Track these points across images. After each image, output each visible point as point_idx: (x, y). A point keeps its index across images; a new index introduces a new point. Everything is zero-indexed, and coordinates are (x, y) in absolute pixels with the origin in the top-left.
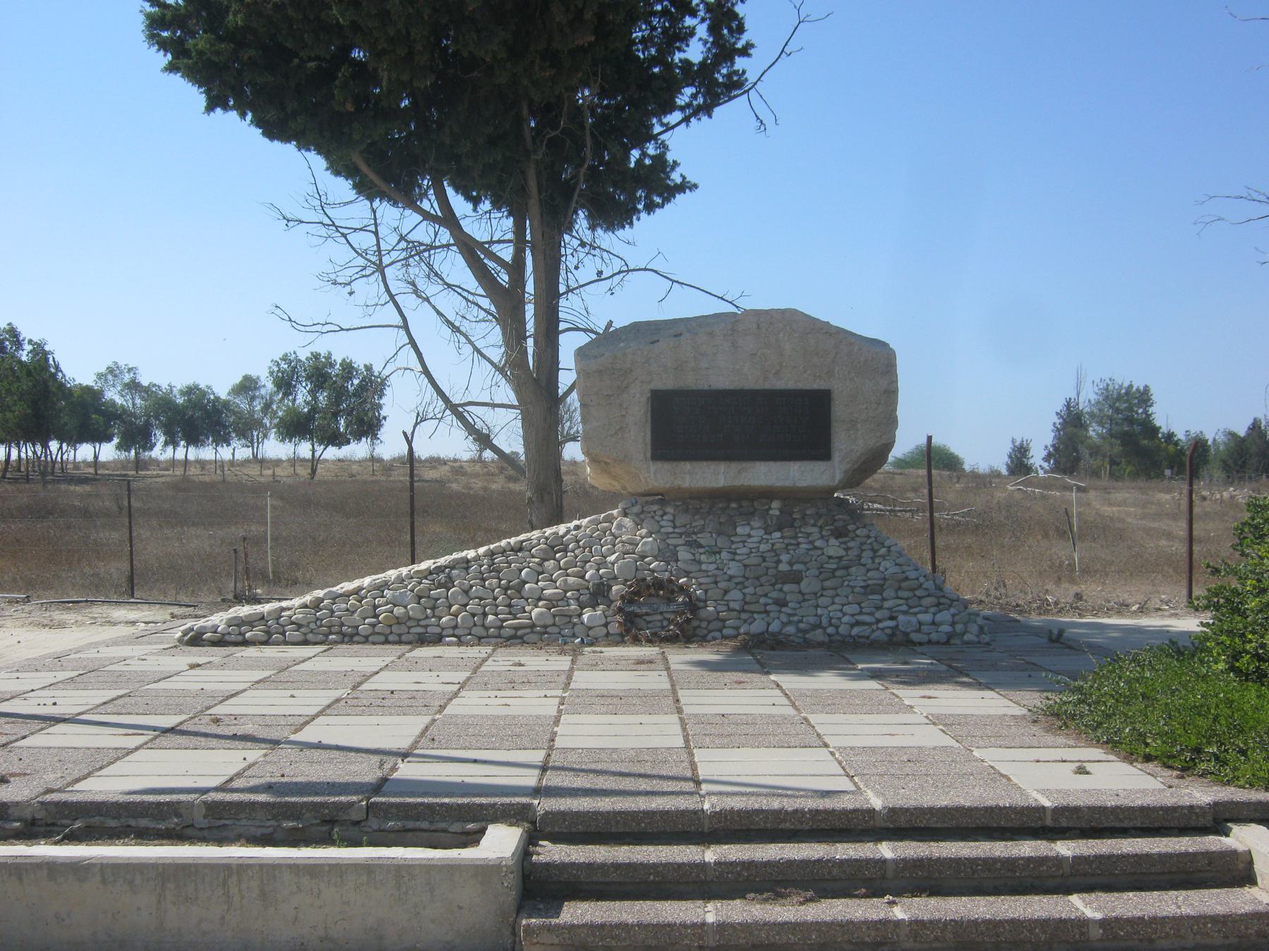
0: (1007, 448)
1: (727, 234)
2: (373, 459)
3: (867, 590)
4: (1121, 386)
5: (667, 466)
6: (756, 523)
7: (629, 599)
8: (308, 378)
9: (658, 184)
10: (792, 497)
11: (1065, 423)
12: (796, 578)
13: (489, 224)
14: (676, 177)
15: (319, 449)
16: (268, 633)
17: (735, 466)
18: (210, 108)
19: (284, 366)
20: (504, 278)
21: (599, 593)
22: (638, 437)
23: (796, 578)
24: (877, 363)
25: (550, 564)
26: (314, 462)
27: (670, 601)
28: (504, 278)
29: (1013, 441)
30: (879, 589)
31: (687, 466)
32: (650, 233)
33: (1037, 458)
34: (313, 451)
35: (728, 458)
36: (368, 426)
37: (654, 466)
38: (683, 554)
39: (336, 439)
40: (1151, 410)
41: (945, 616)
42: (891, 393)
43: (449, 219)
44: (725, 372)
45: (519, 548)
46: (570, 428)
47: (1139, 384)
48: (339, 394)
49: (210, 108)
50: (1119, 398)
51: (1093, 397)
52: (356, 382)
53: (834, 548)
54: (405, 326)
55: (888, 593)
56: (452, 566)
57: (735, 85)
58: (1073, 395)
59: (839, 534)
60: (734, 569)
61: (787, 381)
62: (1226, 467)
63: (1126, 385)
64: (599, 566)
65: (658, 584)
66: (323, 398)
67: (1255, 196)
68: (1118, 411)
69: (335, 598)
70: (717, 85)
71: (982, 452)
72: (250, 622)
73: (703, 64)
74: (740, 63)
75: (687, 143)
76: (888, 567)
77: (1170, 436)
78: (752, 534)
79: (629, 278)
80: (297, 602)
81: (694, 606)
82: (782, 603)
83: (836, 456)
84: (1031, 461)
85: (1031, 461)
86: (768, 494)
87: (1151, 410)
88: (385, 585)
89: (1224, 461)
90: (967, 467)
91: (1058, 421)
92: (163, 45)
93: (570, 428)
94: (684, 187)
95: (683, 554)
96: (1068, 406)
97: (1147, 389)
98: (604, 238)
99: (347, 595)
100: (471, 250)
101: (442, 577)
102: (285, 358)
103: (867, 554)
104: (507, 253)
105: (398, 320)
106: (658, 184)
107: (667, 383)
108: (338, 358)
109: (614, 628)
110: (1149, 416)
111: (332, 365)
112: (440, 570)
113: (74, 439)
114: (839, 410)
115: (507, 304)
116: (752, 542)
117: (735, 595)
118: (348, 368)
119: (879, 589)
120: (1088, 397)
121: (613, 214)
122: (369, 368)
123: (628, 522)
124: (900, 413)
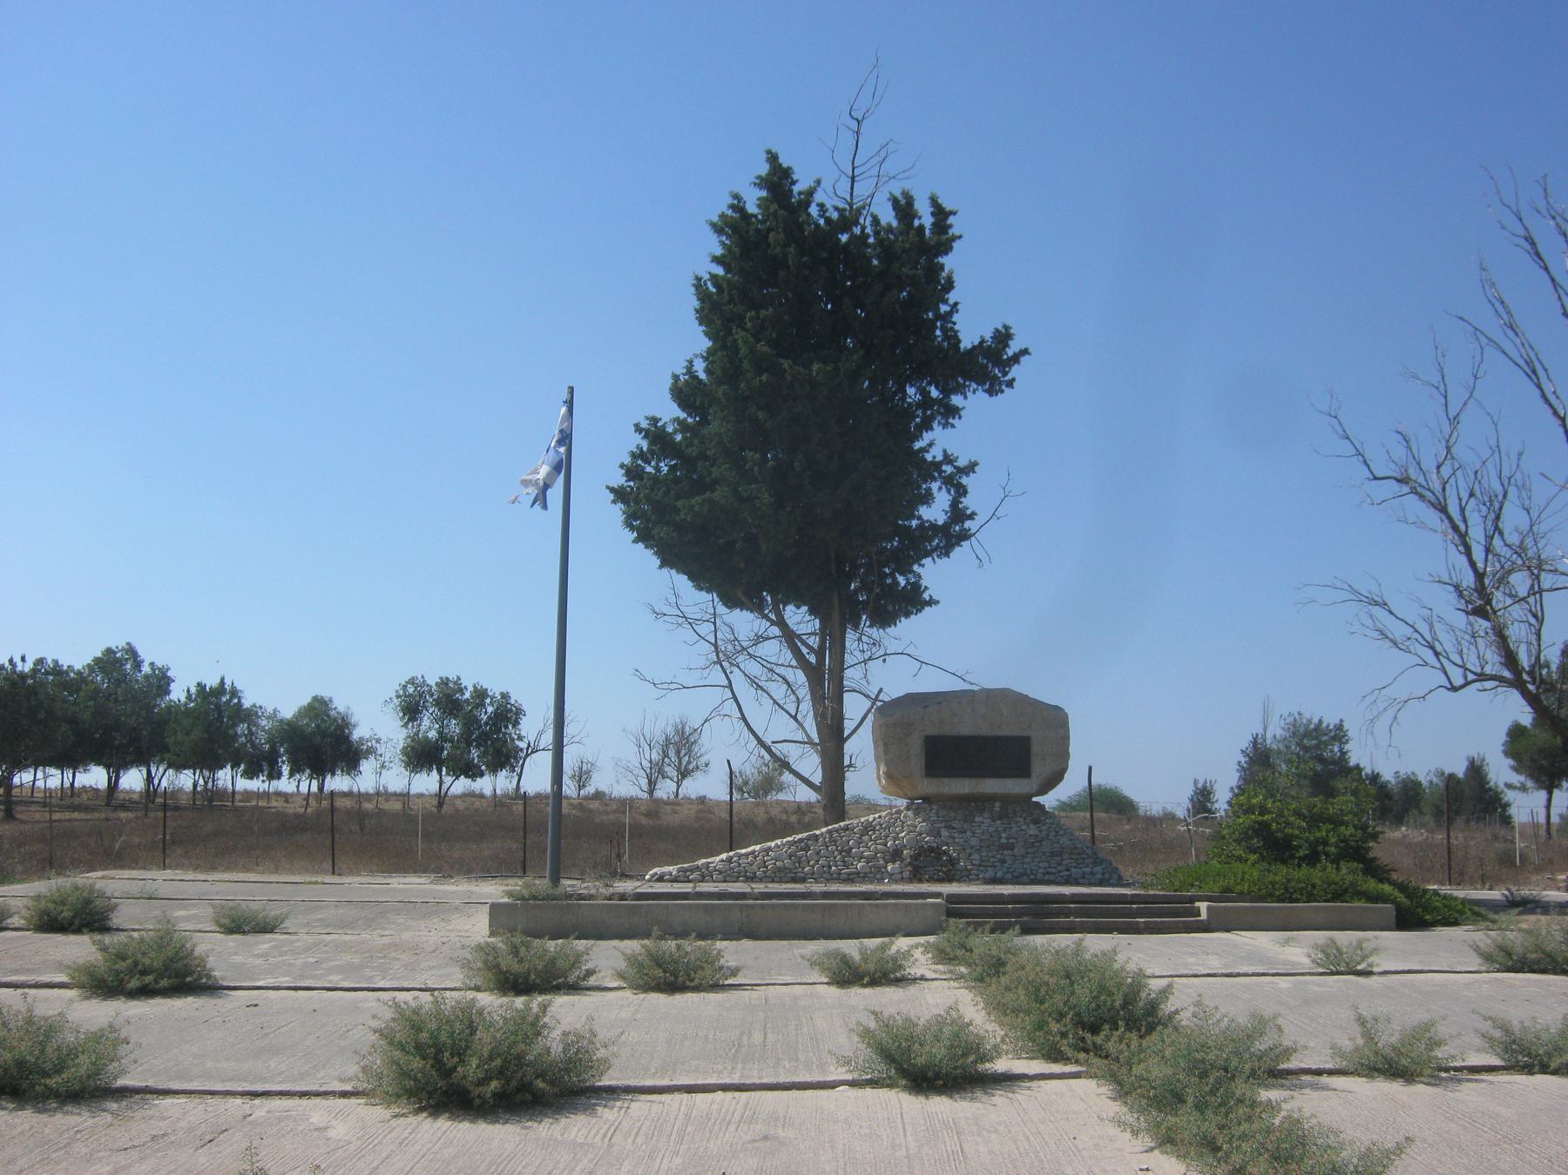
0: (1189, 791)
1: (954, 638)
2: (520, 796)
3: (1053, 854)
4: (1310, 721)
5: (935, 781)
6: (986, 815)
7: (915, 858)
8: (437, 703)
9: (913, 600)
10: (1007, 800)
11: (1252, 761)
12: (1012, 847)
13: (799, 618)
14: (926, 596)
15: (448, 780)
16: (703, 876)
17: (974, 781)
18: (661, 567)
19: (411, 690)
20: (812, 659)
21: (896, 855)
22: (917, 763)
23: (1012, 847)
24: (1056, 720)
25: (866, 838)
27: (938, 858)
28: (812, 659)
29: (1196, 782)
30: (1060, 854)
31: (946, 780)
33: (1221, 801)
34: (441, 782)
35: (971, 776)
36: (504, 756)
37: (926, 781)
38: (944, 833)
39: (471, 771)
40: (1347, 747)
41: (1098, 869)
42: (1066, 738)
43: (781, 623)
45: (846, 829)
46: (689, 762)
47: (1330, 720)
48: (470, 722)
49: (661, 567)
50: (1307, 734)
51: (1279, 733)
52: (490, 709)
53: (1033, 830)
54: (730, 686)
55: (1066, 856)
56: (808, 838)
57: (965, 536)
58: (1260, 731)
59: (1036, 822)
60: (974, 842)
62: (1438, 813)
63: (1315, 720)
64: (895, 839)
65: (931, 849)
66: (454, 727)
67: (1338, 584)
68: (1306, 749)
69: (740, 856)
70: (952, 535)
71: (1160, 792)
72: (692, 870)
73: (945, 523)
74: (968, 524)
75: (932, 573)
76: (1065, 841)
77: (1375, 778)
78: (984, 822)
79: (899, 662)
80: (718, 859)
81: (952, 861)
82: (1003, 861)
83: (1034, 775)
84: (1216, 806)
85: (1216, 806)
86: (992, 798)
87: (1347, 747)
88: (770, 849)
89: (1437, 807)
90: (1141, 812)
91: (1243, 760)
92: (632, 528)
93: (689, 762)
94: (931, 602)
95: (944, 833)
96: (1255, 742)
97: (1340, 727)
98: (874, 632)
99: (747, 855)
100: (790, 638)
101: (804, 846)
102: (412, 681)
103: (1052, 834)
104: (814, 641)
105: (726, 683)
106: (913, 600)
108: (468, 683)
109: (906, 874)
110: (1343, 754)
111: (461, 691)
112: (801, 840)
113: (70, 759)
114: (1036, 748)
115: (815, 674)
116: (984, 827)
117: (976, 856)
118: (481, 694)
119: (1060, 854)
120: (1275, 732)
121: (884, 619)
122: (505, 696)
123: (910, 813)
124: (1071, 750)
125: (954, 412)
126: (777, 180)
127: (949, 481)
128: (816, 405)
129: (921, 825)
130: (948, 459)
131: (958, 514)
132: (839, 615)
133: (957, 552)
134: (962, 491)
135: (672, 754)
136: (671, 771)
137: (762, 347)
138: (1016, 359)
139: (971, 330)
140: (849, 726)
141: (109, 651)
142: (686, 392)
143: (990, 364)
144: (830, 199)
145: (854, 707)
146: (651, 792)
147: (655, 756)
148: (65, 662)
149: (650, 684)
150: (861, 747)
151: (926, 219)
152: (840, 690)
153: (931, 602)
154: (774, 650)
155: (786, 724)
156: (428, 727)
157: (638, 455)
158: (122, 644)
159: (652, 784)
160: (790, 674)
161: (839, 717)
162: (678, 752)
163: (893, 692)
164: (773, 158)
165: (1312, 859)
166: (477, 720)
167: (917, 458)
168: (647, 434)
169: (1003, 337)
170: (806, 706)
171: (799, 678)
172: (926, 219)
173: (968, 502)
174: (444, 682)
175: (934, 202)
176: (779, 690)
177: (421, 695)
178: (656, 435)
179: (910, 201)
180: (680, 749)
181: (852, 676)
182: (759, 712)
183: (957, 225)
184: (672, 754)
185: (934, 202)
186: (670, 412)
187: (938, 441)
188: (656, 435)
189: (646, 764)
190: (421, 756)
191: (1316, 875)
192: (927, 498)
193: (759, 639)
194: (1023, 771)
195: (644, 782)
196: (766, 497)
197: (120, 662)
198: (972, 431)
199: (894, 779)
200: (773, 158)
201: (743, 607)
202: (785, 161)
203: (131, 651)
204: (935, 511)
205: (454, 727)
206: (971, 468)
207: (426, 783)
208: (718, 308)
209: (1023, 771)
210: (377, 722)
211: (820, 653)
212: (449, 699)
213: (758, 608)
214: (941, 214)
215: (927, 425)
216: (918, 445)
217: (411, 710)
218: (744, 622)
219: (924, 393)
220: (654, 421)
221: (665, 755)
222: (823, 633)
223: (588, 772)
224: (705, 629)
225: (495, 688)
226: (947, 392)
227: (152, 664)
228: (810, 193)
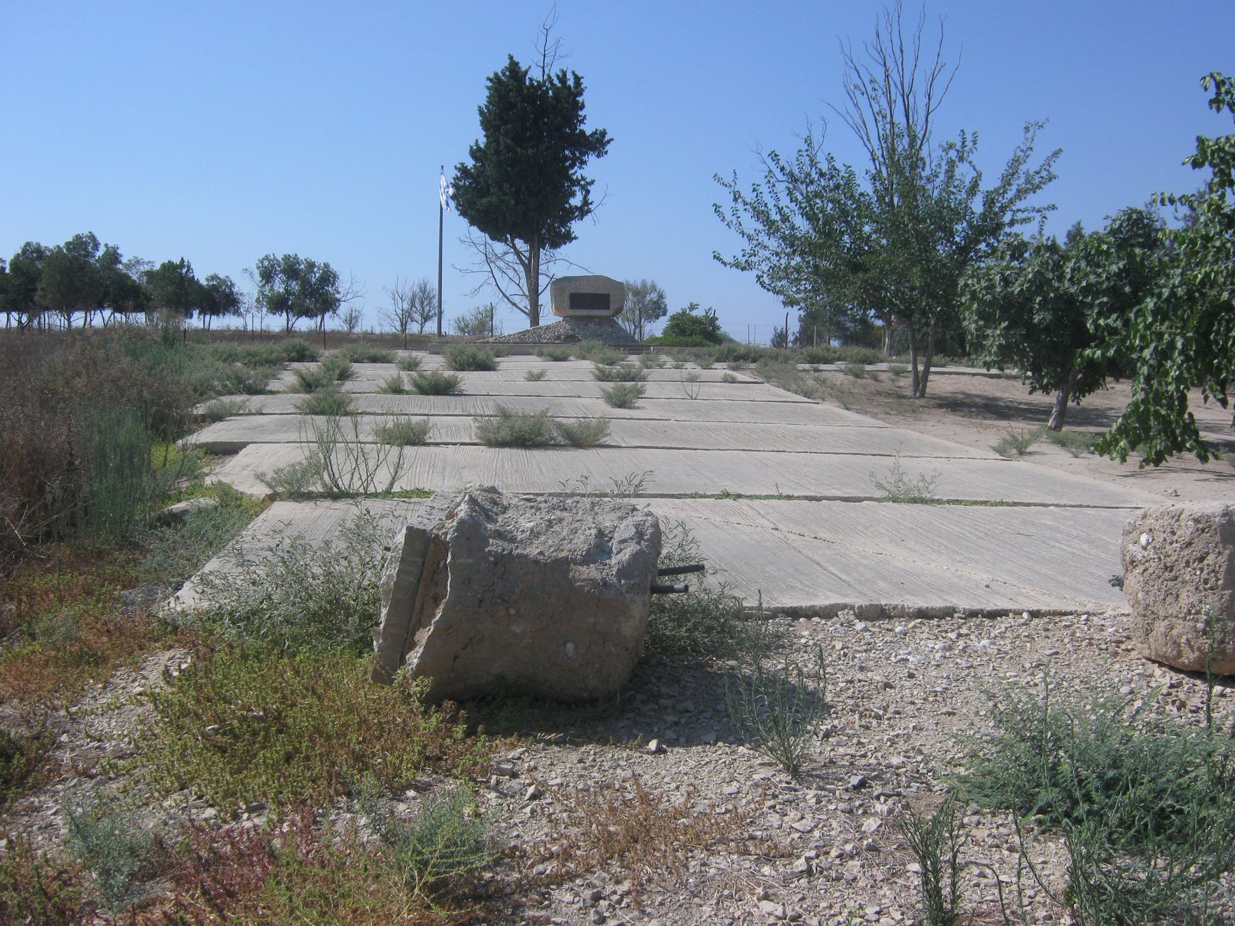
1: (587, 253)
8: (282, 271)
9: (568, 237)
10: (600, 318)
13: (519, 243)
19: (266, 263)
22: (567, 303)
26: (289, 332)
32: (565, 250)
43: (514, 247)
44: (586, 290)
48: (305, 283)
57: (589, 211)
61: (601, 292)
66: (295, 286)
70: (584, 210)
75: (576, 226)
78: (592, 325)
79: (562, 263)
94: (576, 238)
100: (517, 253)
102: (267, 258)
104: (527, 254)
106: (568, 237)
107: (573, 291)
108: (302, 257)
113: (67, 308)
114: (612, 298)
115: (527, 268)
118: (311, 265)
121: (555, 245)
122: (327, 265)
125: (585, 163)
126: (513, 66)
127: (583, 187)
128: (528, 161)
129: (568, 327)
130: (583, 179)
131: (586, 202)
132: (537, 243)
133: (585, 218)
134: (588, 192)
135: (417, 304)
136: (417, 317)
137: (509, 141)
138: (609, 142)
139: (588, 128)
140: (540, 289)
141: (78, 237)
142: (476, 153)
143: (598, 143)
144: (536, 75)
145: (543, 281)
146: (404, 330)
147: (406, 306)
148: (43, 245)
149: (478, 279)
150: (545, 299)
151: (571, 82)
152: (538, 274)
153: (576, 238)
154: (511, 257)
155: (515, 285)
156: (279, 287)
157: (456, 178)
158: (86, 233)
159: (404, 325)
160: (516, 267)
161: (537, 285)
162: (422, 303)
163: (559, 276)
164: (511, 58)
165: (691, 335)
166: (309, 282)
167: (569, 178)
168: (459, 170)
169: (604, 133)
170: (524, 281)
171: (520, 268)
172: (571, 82)
173: (591, 198)
174: (287, 258)
175: (573, 73)
176: (511, 273)
177: (273, 266)
178: (464, 170)
179: (564, 74)
180: (426, 302)
181: (542, 268)
182: (504, 283)
183: (585, 83)
184: (417, 304)
185: (573, 73)
186: (470, 163)
187: (577, 172)
188: (464, 170)
189: (399, 312)
190: (278, 304)
191: (690, 339)
192: (573, 194)
193: (505, 253)
194: (607, 307)
195: (398, 324)
196: (512, 202)
197: (86, 244)
198: (592, 168)
199: (558, 309)
200: (511, 58)
201: (499, 240)
202: (516, 59)
203: (93, 238)
204: (576, 201)
205: (295, 286)
206: (592, 182)
207: (276, 323)
208: (490, 121)
209: (607, 307)
210: (248, 287)
211: (530, 260)
212: (292, 269)
213: (506, 241)
214: (578, 79)
215: (572, 166)
216: (571, 172)
217: (267, 275)
218: (499, 247)
219: (574, 154)
220: (462, 164)
221: (413, 305)
222: (531, 250)
223: (356, 318)
224: (482, 248)
225: (319, 260)
226: (583, 154)
227: (106, 245)
228: (526, 72)
